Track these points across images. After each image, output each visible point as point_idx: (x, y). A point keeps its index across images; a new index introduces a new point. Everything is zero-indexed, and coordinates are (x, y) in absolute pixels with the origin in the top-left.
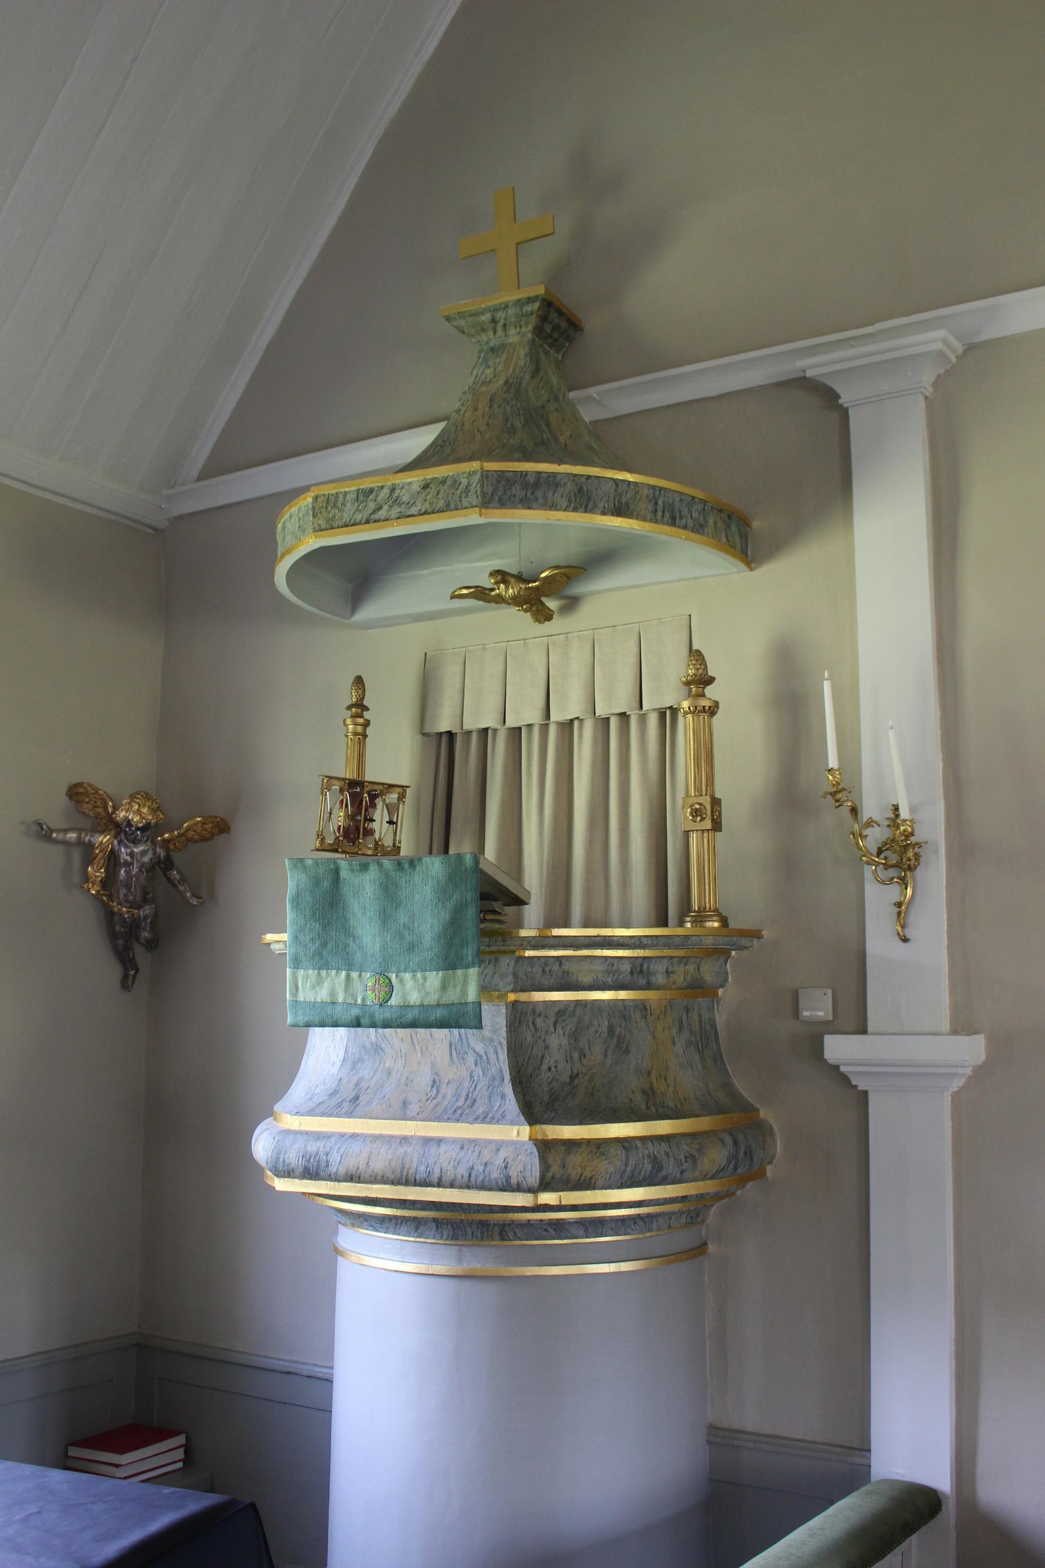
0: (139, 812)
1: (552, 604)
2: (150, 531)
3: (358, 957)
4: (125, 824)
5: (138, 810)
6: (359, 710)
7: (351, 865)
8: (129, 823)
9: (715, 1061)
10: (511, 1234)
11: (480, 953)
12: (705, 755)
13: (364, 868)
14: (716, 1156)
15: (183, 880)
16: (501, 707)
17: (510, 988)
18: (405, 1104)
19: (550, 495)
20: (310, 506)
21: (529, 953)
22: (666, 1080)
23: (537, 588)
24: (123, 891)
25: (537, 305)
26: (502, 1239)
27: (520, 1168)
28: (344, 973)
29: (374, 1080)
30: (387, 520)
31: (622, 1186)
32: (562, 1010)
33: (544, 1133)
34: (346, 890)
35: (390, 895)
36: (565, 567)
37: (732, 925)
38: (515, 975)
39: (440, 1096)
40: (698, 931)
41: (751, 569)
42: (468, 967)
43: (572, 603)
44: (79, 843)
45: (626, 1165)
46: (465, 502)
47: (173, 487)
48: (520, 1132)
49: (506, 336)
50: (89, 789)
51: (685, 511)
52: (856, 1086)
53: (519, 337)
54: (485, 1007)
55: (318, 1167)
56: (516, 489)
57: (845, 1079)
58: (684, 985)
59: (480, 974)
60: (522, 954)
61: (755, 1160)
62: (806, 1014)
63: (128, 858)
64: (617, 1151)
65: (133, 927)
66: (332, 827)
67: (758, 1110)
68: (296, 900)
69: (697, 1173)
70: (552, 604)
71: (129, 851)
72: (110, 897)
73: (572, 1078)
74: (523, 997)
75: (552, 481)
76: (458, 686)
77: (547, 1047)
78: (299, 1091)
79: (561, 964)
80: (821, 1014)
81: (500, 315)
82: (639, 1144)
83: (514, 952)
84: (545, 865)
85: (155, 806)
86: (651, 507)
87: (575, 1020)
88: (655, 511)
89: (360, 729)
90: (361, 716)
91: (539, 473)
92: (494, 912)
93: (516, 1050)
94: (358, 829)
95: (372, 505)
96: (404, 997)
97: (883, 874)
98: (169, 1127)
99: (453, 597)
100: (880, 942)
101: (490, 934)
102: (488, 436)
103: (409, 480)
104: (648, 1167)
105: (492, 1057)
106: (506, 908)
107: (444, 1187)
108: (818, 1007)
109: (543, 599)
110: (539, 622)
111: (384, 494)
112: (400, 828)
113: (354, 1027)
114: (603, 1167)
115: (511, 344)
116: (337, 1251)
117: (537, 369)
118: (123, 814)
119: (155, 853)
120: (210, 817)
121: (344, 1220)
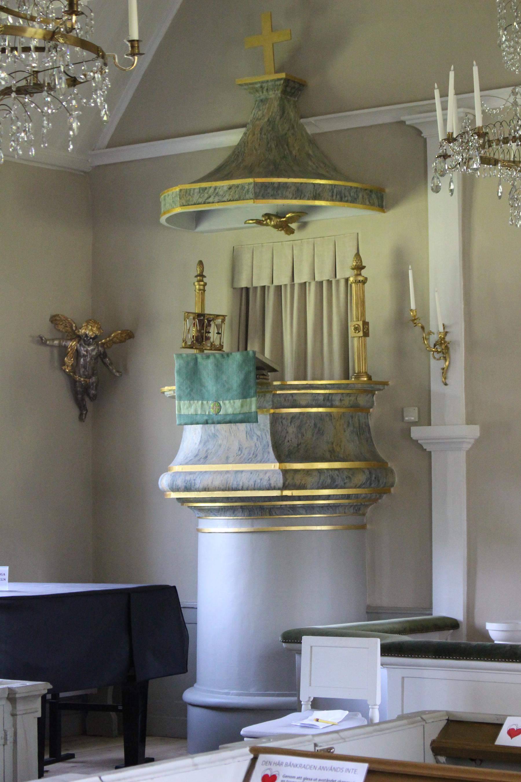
0: (92, 330)
1: (294, 226)
2: (82, 173)
3: (206, 395)
4: (84, 336)
5: (91, 329)
6: (201, 278)
7: (202, 356)
8: (86, 336)
9: (367, 441)
10: (274, 513)
11: (256, 392)
12: (362, 303)
13: (208, 357)
14: (361, 478)
15: (111, 364)
16: (271, 276)
17: (271, 406)
18: (227, 458)
19: (285, 192)
20: (178, 193)
21: (278, 392)
22: (340, 446)
23: (285, 221)
24: (82, 370)
25: (282, 82)
26: (270, 515)
27: (275, 479)
28: (200, 402)
29: (214, 449)
30: (213, 203)
31: (318, 488)
32: (294, 416)
33: (286, 467)
34: (201, 367)
35: (219, 368)
36: (298, 212)
37: (374, 379)
38: (273, 401)
39: (242, 455)
40: (357, 382)
41: (384, 212)
42: (252, 397)
43: (303, 225)
44: (60, 346)
45: (320, 479)
46: (247, 196)
47: (93, 150)
48: (275, 466)
49: (268, 94)
50: (62, 318)
51: (347, 194)
52: (426, 449)
53: (274, 95)
54: (259, 413)
55: (191, 485)
56: (270, 190)
57: (421, 446)
58: (349, 406)
59: (257, 400)
60: (275, 392)
61: (381, 482)
62: (406, 419)
63: (85, 353)
64: (315, 473)
65: (86, 389)
66: (190, 336)
67: (387, 463)
68: (179, 372)
69: (352, 485)
70: (294, 226)
71: (85, 349)
72: (75, 373)
73: (298, 445)
74: (277, 411)
75: (285, 186)
76: (250, 264)
77: (287, 432)
78: (180, 456)
79: (292, 397)
80: (413, 418)
81: (264, 85)
82: (325, 471)
83: (272, 392)
84: (294, 352)
85: (99, 326)
86: (330, 194)
87: (299, 421)
88: (332, 196)
89: (202, 287)
90: (202, 281)
91: (279, 183)
92: (264, 375)
93: (274, 434)
94: (202, 337)
95: (206, 195)
96: (226, 411)
97: (437, 355)
98: (106, 491)
99: (245, 223)
100: (436, 386)
101: (261, 384)
102: (259, 152)
103: (222, 185)
104: (329, 481)
105: (264, 436)
106: (269, 373)
107: (244, 490)
108: (412, 415)
109: (289, 225)
110: (288, 234)
111: (212, 190)
112: (223, 336)
113: (205, 424)
114: (310, 480)
115: (271, 98)
116: (198, 530)
117: (283, 113)
118: (83, 331)
119: (98, 350)
120: (125, 330)
121: (201, 514)
